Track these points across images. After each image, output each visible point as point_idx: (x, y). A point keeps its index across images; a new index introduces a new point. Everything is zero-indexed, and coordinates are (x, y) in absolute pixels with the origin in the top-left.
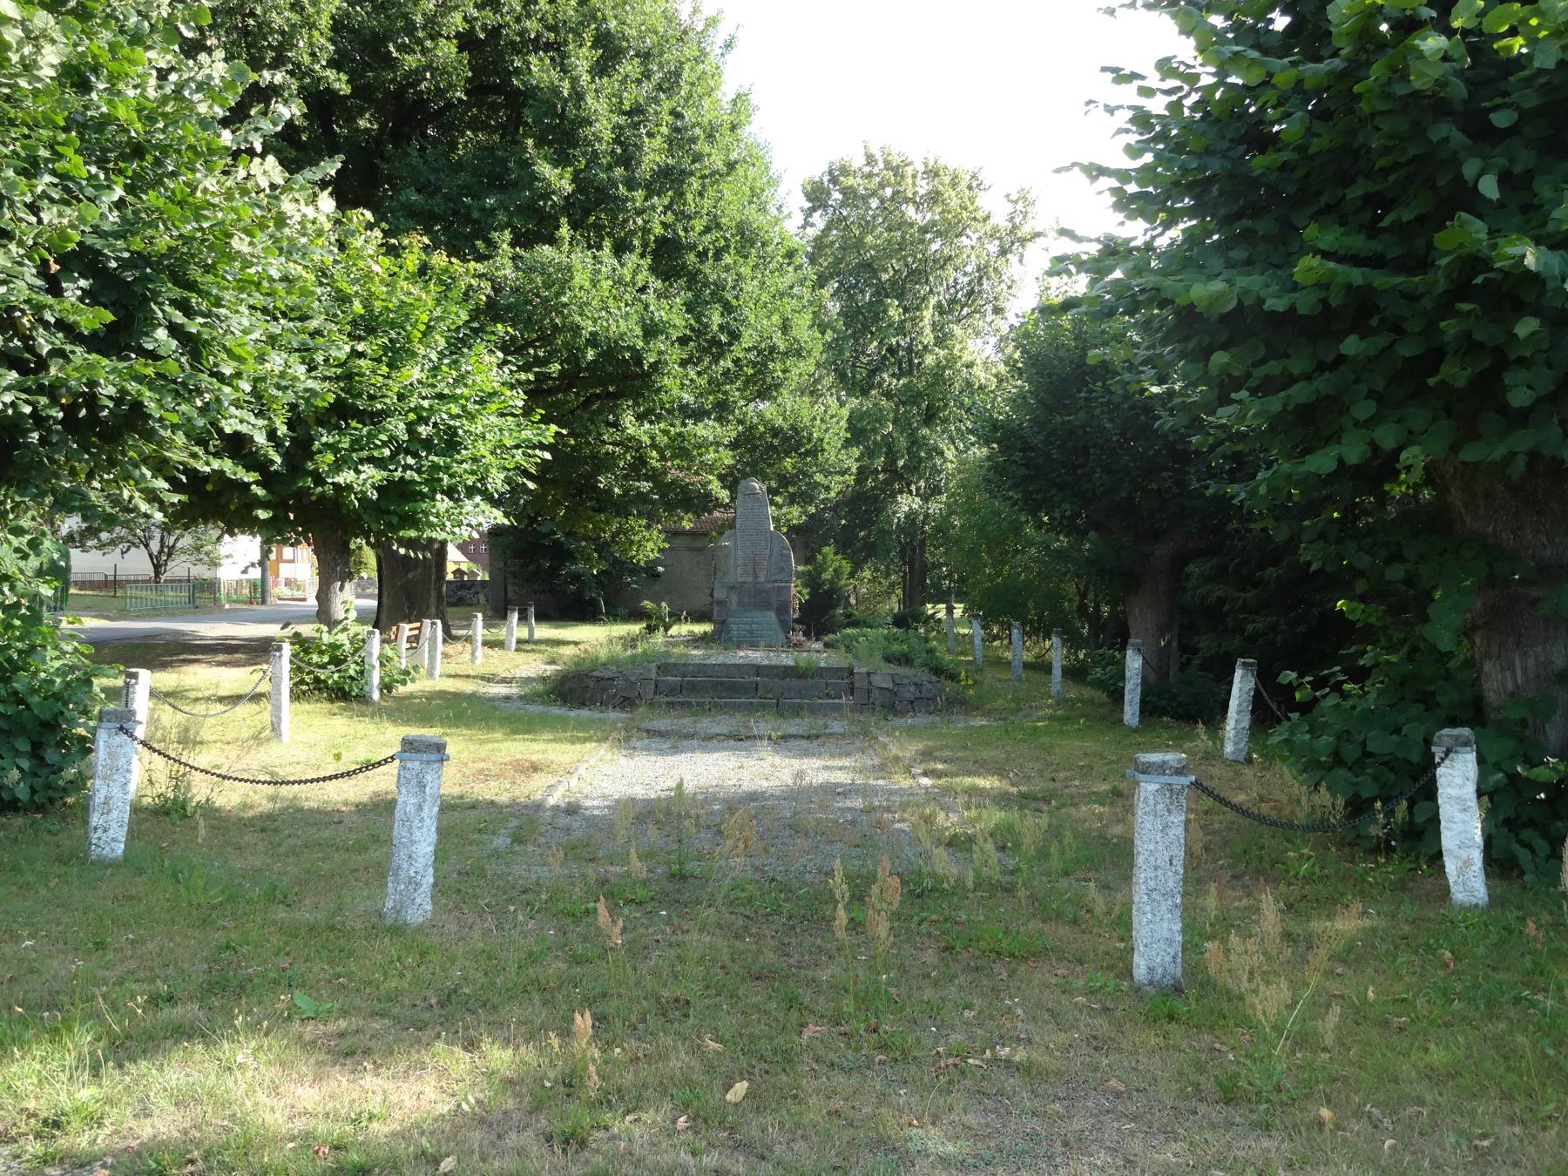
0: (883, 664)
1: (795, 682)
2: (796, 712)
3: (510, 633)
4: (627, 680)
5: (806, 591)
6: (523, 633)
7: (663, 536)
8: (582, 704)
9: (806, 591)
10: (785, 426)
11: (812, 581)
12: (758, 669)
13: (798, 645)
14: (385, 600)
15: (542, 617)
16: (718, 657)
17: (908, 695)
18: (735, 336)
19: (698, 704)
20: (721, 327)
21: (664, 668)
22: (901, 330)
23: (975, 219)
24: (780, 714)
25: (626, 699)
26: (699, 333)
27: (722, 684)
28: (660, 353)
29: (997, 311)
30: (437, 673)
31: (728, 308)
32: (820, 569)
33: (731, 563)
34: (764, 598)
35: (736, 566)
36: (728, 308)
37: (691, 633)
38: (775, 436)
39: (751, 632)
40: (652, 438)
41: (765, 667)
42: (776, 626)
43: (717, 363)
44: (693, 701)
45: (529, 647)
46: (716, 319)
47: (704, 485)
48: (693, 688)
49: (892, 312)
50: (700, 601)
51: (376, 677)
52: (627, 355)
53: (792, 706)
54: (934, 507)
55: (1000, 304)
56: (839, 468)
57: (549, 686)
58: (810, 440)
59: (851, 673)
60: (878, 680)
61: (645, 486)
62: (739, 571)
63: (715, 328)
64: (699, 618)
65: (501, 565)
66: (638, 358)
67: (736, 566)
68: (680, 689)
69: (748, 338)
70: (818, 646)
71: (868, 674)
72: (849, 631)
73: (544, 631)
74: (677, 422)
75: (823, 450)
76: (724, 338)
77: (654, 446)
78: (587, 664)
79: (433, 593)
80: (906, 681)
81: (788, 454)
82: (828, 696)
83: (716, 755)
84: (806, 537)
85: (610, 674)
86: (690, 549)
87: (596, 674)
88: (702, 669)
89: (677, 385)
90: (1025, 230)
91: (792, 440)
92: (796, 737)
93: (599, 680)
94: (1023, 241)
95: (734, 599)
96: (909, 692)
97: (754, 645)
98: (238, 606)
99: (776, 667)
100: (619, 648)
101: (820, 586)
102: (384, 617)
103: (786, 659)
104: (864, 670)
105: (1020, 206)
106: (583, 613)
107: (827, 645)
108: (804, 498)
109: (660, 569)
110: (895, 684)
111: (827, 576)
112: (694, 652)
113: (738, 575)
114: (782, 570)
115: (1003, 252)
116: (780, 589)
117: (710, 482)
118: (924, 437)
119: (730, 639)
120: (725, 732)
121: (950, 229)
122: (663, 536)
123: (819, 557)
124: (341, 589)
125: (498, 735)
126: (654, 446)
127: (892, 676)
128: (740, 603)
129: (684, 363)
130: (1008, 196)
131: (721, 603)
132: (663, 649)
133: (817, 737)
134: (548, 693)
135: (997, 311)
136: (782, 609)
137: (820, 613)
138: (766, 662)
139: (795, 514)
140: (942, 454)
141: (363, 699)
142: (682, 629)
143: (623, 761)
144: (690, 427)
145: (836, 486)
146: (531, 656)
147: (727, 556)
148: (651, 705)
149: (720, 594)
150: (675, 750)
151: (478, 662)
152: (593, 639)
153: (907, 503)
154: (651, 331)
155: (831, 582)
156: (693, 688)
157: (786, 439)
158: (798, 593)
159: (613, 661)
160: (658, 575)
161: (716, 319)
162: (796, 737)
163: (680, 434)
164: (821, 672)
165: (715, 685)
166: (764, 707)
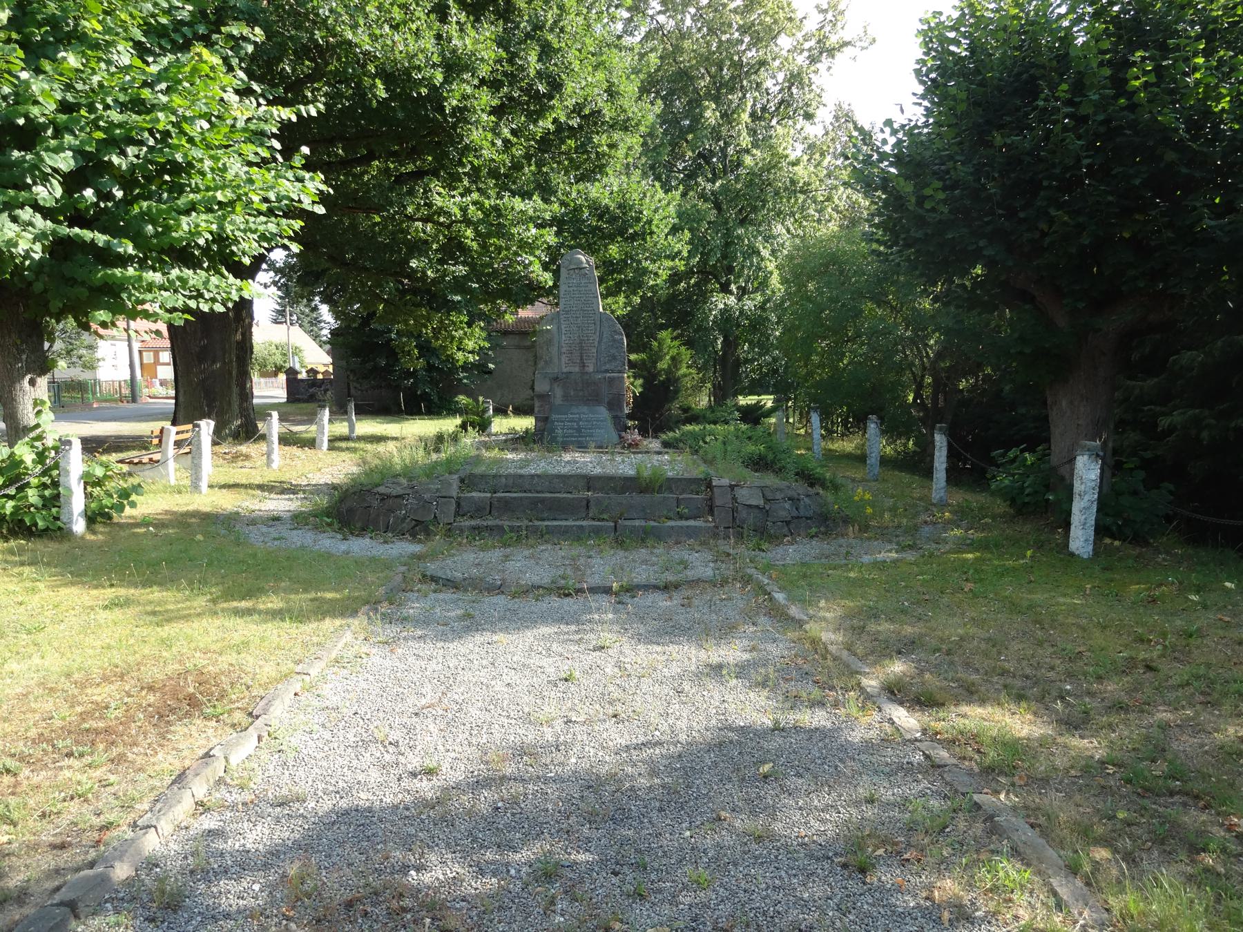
0: (747, 473)
1: (637, 498)
2: (644, 537)
3: (321, 430)
4: (420, 499)
5: (640, 382)
6: (341, 428)
7: (484, 334)
8: (362, 531)
9: (640, 382)
10: (613, 206)
11: (645, 371)
12: (590, 482)
13: (633, 446)
14: (181, 399)
15: (365, 411)
16: (539, 463)
17: (783, 514)
18: (556, 86)
19: (512, 529)
20: (539, 74)
21: (468, 482)
22: (716, 134)
23: (790, 19)
24: (620, 543)
25: (418, 523)
26: (512, 78)
27: (543, 500)
28: (465, 97)
29: (808, 117)
30: (204, 485)
31: (547, 51)
32: (656, 357)
33: (554, 350)
34: (591, 391)
35: (560, 354)
36: (547, 51)
37: (513, 431)
38: (600, 217)
39: (579, 430)
40: (464, 210)
41: (598, 478)
42: (609, 424)
43: (535, 122)
44: (506, 524)
45: (343, 445)
46: (532, 60)
47: (526, 267)
48: (507, 507)
49: (708, 114)
50: (523, 396)
51: (78, 503)
52: (424, 91)
53: (633, 530)
54: (749, 304)
55: (811, 110)
56: (667, 254)
57: (323, 501)
58: (638, 220)
59: (709, 486)
60: (744, 495)
61: (461, 270)
62: (564, 359)
63: (532, 73)
64: (520, 411)
65: (344, 363)
66: (436, 98)
67: (560, 354)
68: (489, 508)
69: (573, 90)
70: (655, 445)
71: (732, 487)
72: (689, 428)
73: (367, 427)
74: (492, 193)
75: (652, 233)
76: (542, 88)
77: (467, 221)
78: (376, 478)
79: (235, 390)
80: (779, 496)
81: (612, 238)
82: (681, 517)
83: (529, 636)
84: (637, 330)
85: (398, 490)
86: (518, 347)
87: (382, 489)
88: (517, 482)
89: (484, 140)
90: (833, 40)
91: (619, 224)
92: (647, 587)
93: (385, 498)
94: (831, 52)
95: (559, 392)
96: (784, 510)
97: (582, 447)
98: (104, 405)
99: (611, 478)
100: (421, 452)
101: (654, 376)
102: (180, 416)
103: (624, 465)
104: (725, 482)
105: (829, 16)
106: (416, 406)
107: (666, 445)
108: (635, 285)
109: (491, 366)
110: (767, 500)
111: (663, 365)
112: (510, 456)
113: (564, 365)
114: (614, 358)
115: (813, 60)
116: (611, 380)
117: (531, 263)
118: (739, 237)
119: (554, 440)
120: (546, 581)
121: (762, 35)
122: (484, 334)
123: (655, 344)
124: (32, 383)
125: (201, 602)
126: (467, 221)
127: (762, 488)
128: (566, 397)
129: (498, 111)
130: (817, 7)
131: (544, 397)
132: (474, 453)
133: (677, 586)
134: (327, 513)
135: (808, 117)
136: (614, 404)
137: (655, 410)
138: (598, 471)
139: (620, 305)
140: (758, 253)
141: (57, 532)
142: (501, 425)
143: (377, 658)
144: (506, 199)
145: (660, 273)
146: (345, 456)
147: (549, 342)
148: (449, 532)
149: (542, 387)
150: (470, 624)
151: (275, 466)
152: (406, 438)
153: (721, 302)
154: (454, 66)
155: (669, 372)
156: (507, 507)
157: (614, 219)
158: (632, 386)
159: (408, 472)
160: (490, 372)
161: (532, 60)
162: (647, 587)
163: (496, 208)
164: (671, 484)
165: (534, 503)
166: (597, 532)
